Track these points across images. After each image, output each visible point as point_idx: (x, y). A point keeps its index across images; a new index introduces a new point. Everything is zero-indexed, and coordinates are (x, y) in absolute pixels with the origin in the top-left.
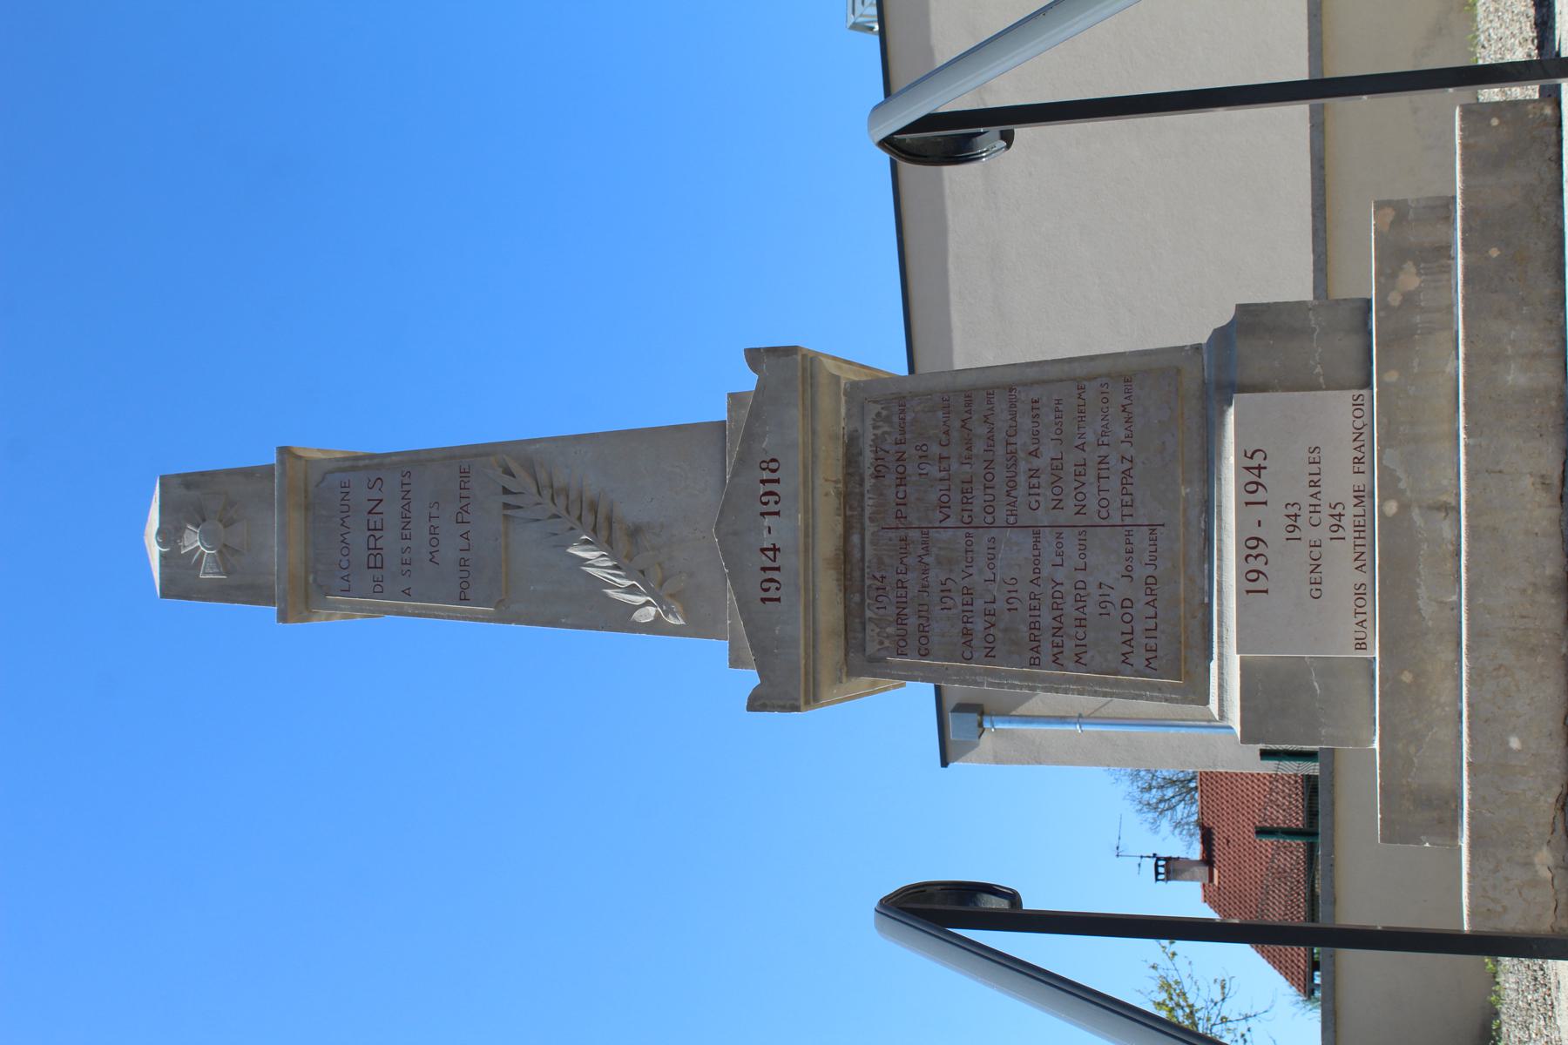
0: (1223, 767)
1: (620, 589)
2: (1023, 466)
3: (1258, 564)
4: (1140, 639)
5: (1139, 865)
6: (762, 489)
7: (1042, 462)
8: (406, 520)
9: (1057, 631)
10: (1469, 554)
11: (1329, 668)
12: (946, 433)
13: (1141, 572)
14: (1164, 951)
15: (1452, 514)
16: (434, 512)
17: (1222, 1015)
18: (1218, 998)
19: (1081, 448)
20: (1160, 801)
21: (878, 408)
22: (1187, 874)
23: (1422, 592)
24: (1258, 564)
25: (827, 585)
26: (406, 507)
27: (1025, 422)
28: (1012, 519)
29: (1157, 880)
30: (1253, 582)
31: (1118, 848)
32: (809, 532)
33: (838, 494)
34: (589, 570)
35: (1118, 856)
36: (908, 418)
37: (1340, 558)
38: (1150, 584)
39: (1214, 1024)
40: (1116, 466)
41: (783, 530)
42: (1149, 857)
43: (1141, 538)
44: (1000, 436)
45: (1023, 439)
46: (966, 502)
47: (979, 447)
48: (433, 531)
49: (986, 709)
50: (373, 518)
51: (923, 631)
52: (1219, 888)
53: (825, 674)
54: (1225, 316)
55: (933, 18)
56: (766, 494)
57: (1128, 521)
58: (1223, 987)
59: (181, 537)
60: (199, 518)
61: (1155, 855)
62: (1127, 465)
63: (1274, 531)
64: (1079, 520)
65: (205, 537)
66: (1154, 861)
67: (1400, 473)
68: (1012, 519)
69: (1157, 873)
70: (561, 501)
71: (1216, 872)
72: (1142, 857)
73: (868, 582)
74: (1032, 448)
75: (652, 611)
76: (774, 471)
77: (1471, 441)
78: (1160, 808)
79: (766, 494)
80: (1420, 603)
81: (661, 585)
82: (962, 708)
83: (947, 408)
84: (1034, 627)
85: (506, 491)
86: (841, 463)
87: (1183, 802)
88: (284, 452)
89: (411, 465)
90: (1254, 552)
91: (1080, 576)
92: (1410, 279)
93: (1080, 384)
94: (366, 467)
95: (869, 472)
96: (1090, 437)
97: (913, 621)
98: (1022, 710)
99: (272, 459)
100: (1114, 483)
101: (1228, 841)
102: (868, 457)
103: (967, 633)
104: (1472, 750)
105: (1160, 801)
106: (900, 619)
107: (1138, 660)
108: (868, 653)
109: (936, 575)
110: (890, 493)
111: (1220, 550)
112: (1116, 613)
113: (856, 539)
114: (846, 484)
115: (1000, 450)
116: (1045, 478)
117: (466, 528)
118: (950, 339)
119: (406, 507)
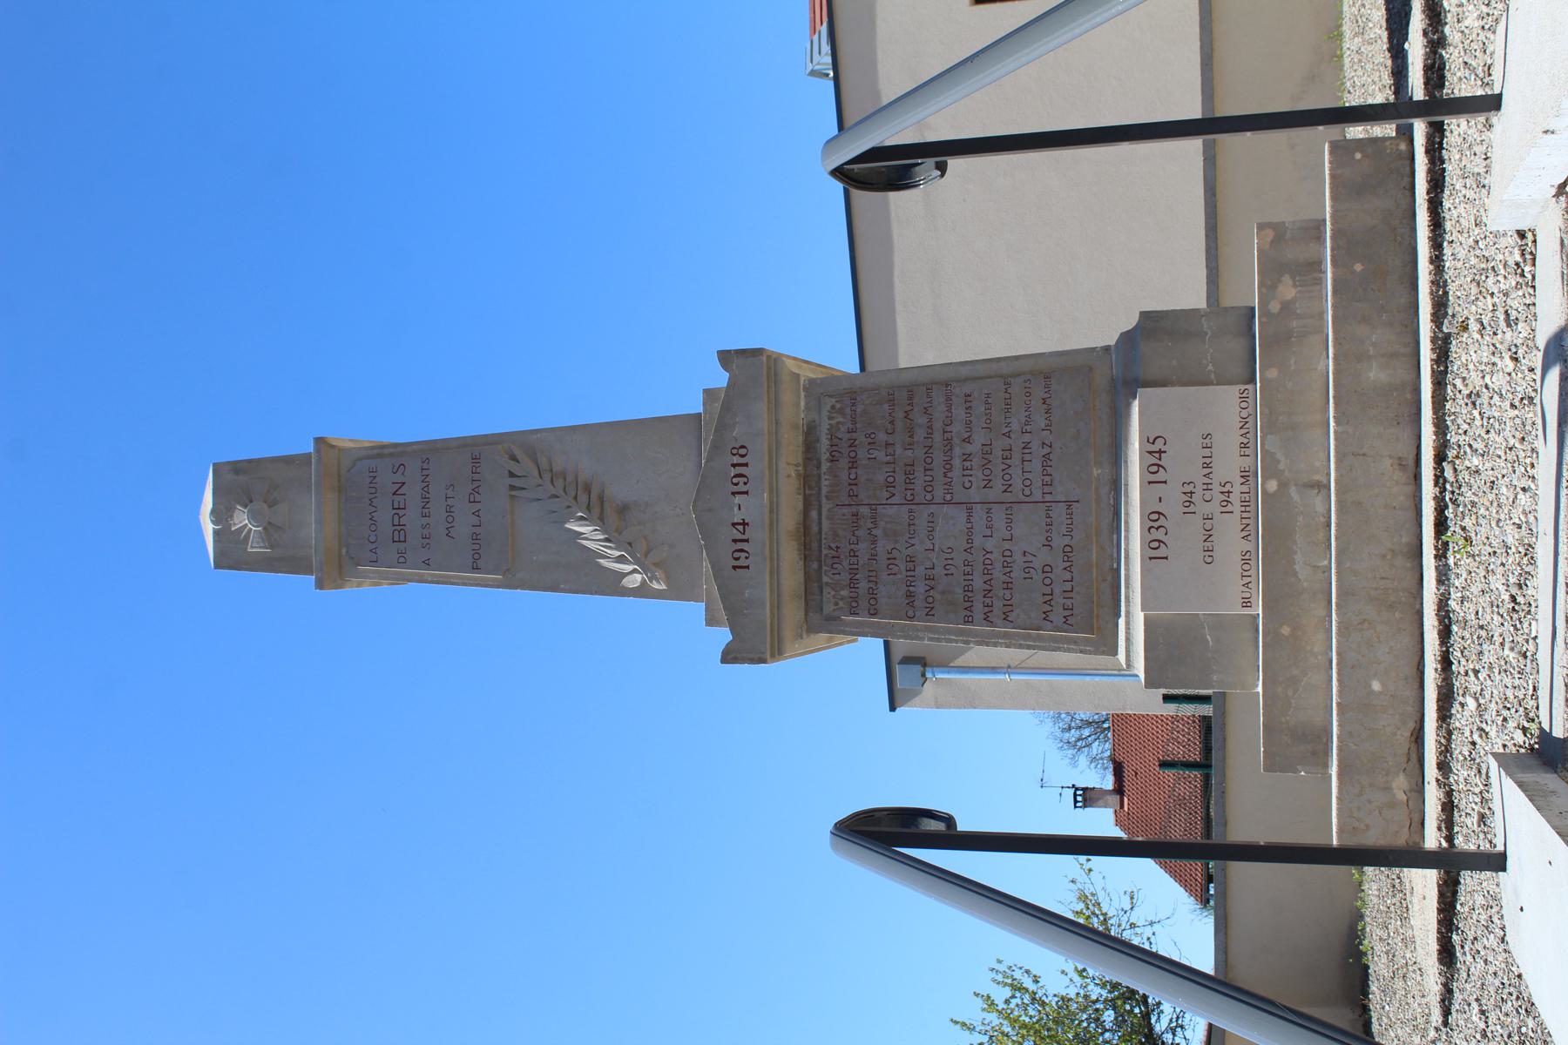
0: (1131, 710)
2: (957, 451)
3: (1159, 535)
4: (1059, 600)
6: (733, 472)
7: (974, 448)
8: (426, 500)
9: (987, 593)
10: (1338, 525)
11: (1220, 623)
12: (892, 422)
13: (1059, 542)
15: (1324, 491)
16: (450, 493)
18: (1127, 907)
19: (1008, 435)
20: (1079, 740)
22: (1101, 802)
23: (1298, 558)
24: (1159, 535)
25: (790, 554)
26: (426, 488)
27: (959, 412)
28: (948, 497)
29: (1075, 807)
30: (1155, 549)
31: (1042, 780)
32: (774, 509)
33: (799, 475)
34: (584, 542)
35: (1042, 787)
38: (1068, 552)
41: (751, 508)
42: (1069, 787)
43: (1059, 512)
44: (938, 425)
45: (957, 428)
47: (920, 435)
48: (449, 510)
49: (929, 660)
51: (872, 594)
52: (1129, 814)
53: (788, 633)
54: (1130, 322)
55: (880, 67)
56: (736, 476)
57: (1048, 498)
58: (1132, 898)
59: (232, 516)
61: (1073, 786)
62: (1047, 450)
63: (1173, 507)
64: (1007, 497)
65: (253, 516)
66: (1073, 791)
67: (1279, 456)
69: (1076, 801)
71: (1126, 800)
72: (1062, 787)
73: (824, 552)
74: (966, 435)
75: (638, 577)
78: (1078, 745)
79: (736, 476)
80: (1297, 567)
83: (892, 401)
84: (968, 589)
85: (512, 475)
86: (801, 449)
88: (320, 441)
89: (429, 453)
90: (1156, 524)
91: (1007, 545)
92: (1287, 290)
93: (1006, 380)
94: (391, 455)
95: (825, 456)
96: (1015, 426)
97: (863, 586)
98: (959, 662)
99: (310, 448)
100: (1036, 465)
102: (824, 443)
103: (910, 595)
104: (1340, 692)
105: (1079, 740)
109: (883, 546)
110: (844, 475)
111: (1127, 523)
112: (1038, 577)
113: (814, 514)
114: (805, 467)
116: (976, 462)
118: (895, 343)
119: (426, 488)
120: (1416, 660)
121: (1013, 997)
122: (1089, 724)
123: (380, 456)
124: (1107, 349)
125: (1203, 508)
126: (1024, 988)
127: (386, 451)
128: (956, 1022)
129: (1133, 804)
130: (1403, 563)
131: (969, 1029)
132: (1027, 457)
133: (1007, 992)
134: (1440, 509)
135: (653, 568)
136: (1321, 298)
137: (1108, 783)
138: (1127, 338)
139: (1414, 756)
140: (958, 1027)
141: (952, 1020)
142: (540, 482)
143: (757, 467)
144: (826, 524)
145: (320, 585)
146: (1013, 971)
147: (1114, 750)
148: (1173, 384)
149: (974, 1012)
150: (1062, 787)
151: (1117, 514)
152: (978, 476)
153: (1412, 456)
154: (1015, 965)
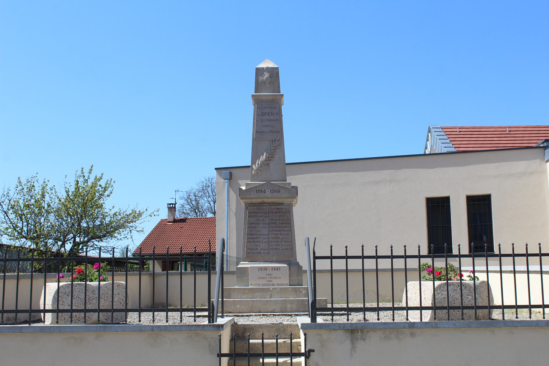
0: (217, 242)
1: (259, 162)
2: (278, 232)
3: (263, 270)
4: (252, 251)
5: (173, 198)
6: (275, 190)
7: (279, 236)
8: (270, 120)
9: (253, 238)
10: (264, 300)
11: (248, 280)
12: (284, 220)
13: (262, 251)
14: (152, 213)
15: (270, 298)
16: (272, 126)
17: (132, 231)
18: (138, 229)
19: (281, 242)
20: (191, 200)
21: (288, 208)
22: (170, 214)
23: (259, 293)
24: (263, 270)
25: (259, 201)
26: (273, 120)
27: (285, 233)
28: (270, 231)
29: (168, 204)
30: (261, 269)
31: (178, 191)
32: (268, 198)
33: (274, 202)
34: (262, 156)
35: (175, 191)
36: (286, 214)
37: (264, 282)
38: (260, 253)
39: (130, 229)
40: (278, 247)
41: (268, 193)
42: (175, 201)
43: (267, 251)
44: (283, 229)
45: (283, 232)
46: (273, 223)
47: (281, 225)
48: (268, 126)
49: (230, 180)
50: (271, 113)
51: (252, 216)
52: (166, 225)
53: (245, 200)
54: (301, 264)
55: (409, 170)
56: (274, 191)
57: (270, 249)
58: (141, 231)
59: (267, 72)
60: (271, 77)
61: (176, 203)
62: (278, 249)
63: (268, 272)
64: (270, 242)
65: (267, 78)
66: (174, 203)
67: (276, 290)
68: (270, 231)
69: (170, 204)
70: (273, 151)
71: (171, 224)
72: (175, 199)
73: (260, 207)
74: (281, 234)
75: (255, 168)
76: (278, 192)
77: (280, 300)
78: (188, 199)
79: (274, 191)
80: (257, 293)
81: (259, 170)
82: (231, 174)
83: (288, 220)
84: (253, 234)
85: (275, 140)
86: (279, 202)
87: (190, 208)
88: (283, 95)
89: (279, 121)
90: (265, 269)
91: (261, 242)
92: (304, 292)
93: (291, 242)
94: (280, 112)
95: (278, 207)
96: (283, 243)
97: (254, 215)
98: (231, 189)
99: (282, 93)
100: (276, 247)
101: (182, 228)
102: (280, 207)
103: (252, 224)
104: (237, 300)
105: (191, 200)
106: (254, 212)
107: (248, 251)
108: (249, 207)
109: (261, 218)
110: (274, 211)
111: (265, 263)
112: (256, 247)
113: (267, 205)
114: (276, 203)
115: (281, 229)
116: (276, 236)
117: (269, 132)
118: (327, 172)
119: (273, 120)
120: (242, 312)
121: (102, 188)
122: (198, 203)
123: (279, 110)
124: (296, 260)
125: (268, 277)
126: (105, 191)
127: (280, 111)
128: (92, 167)
129: (170, 227)
130: (258, 310)
131: (90, 172)
132: (277, 245)
133: (103, 186)
134: (266, 315)
135: (257, 171)
136: (302, 297)
137: (178, 216)
138: (298, 264)
139: (227, 312)
140: (90, 168)
141: (93, 165)
142: (274, 146)
143: (276, 194)
144: (265, 207)
145: (253, 96)
146: (111, 187)
147: (191, 219)
148: (289, 272)
149: (96, 173)
150: (175, 199)
151: (267, 262)
152: (274, 236)
153: (275, 312)
154: (113, 188)
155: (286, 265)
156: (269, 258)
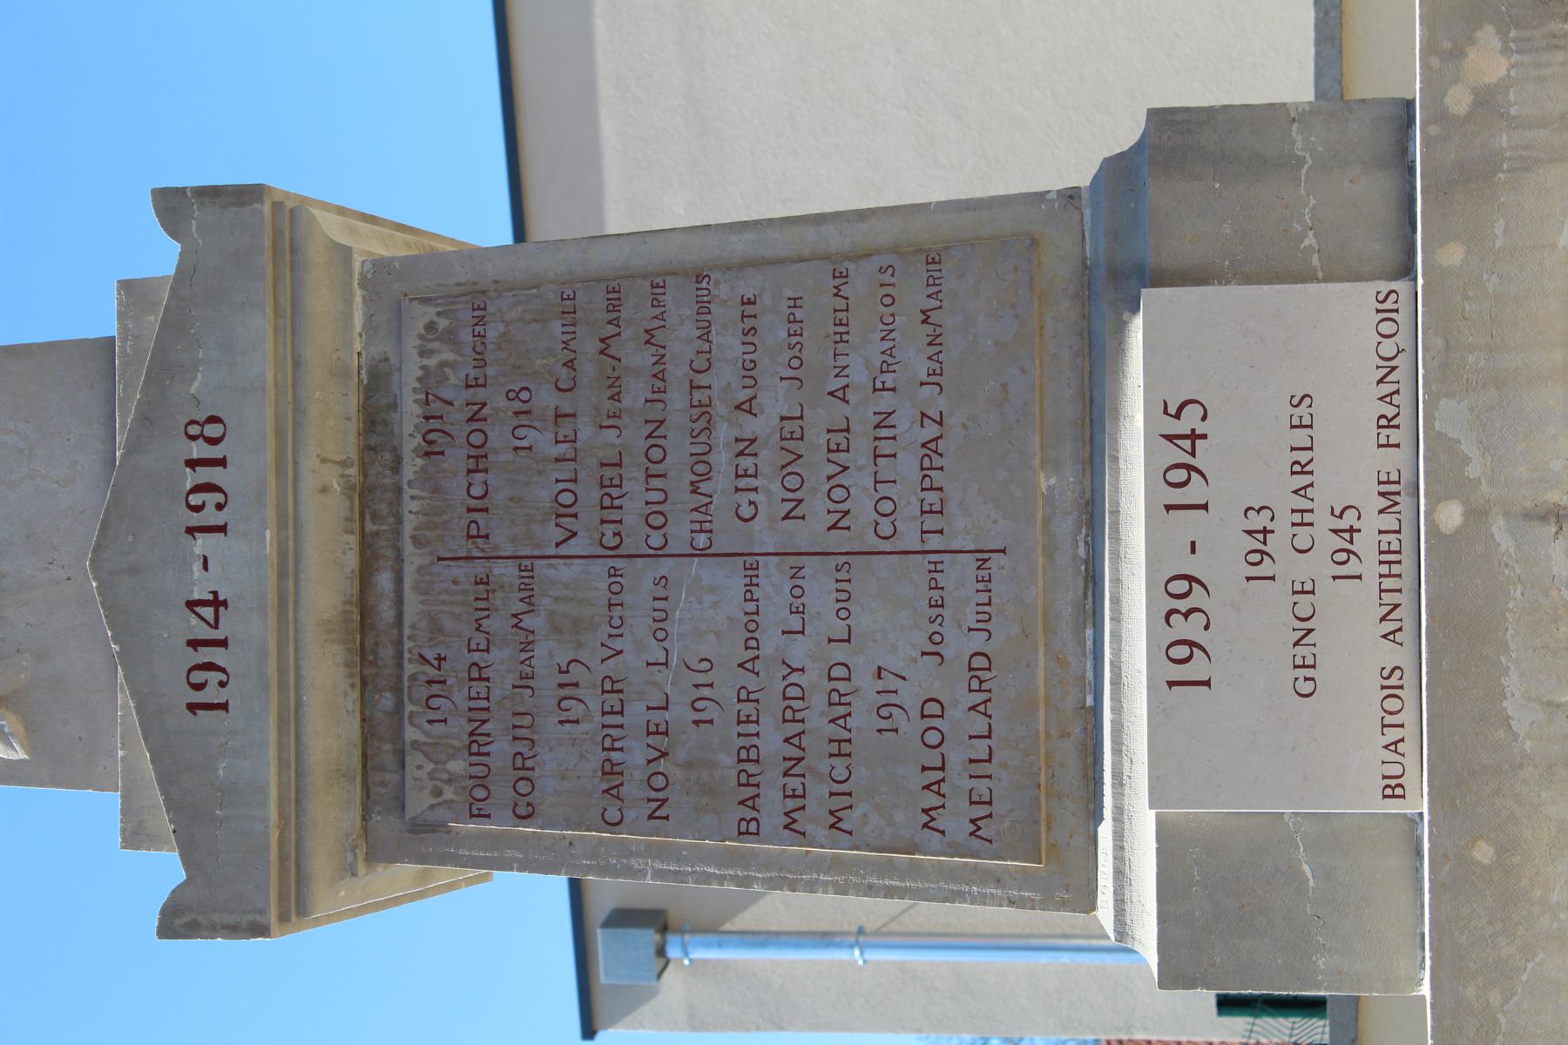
0: (1146, 1029)
2: (723, 433)
3: (1191, 629)
4: (958, 781)
6: (191, 478)
7: (763, 425)
12: (569, 364)
13: (959, 645)
19: (840, 395)
24: (1191, 629)
27: (728, 343)
28: (702, 540)
32: (288, 567)
33: (349, 488)
36: (492, 335)
38: (979, 669)
40: (910, 432)
43: (959, 575)
44: (678, 372)
45: (724, 377)
46: (610, 505)
47: (636, 392)
51: (523, 768)
53: (321, 862)
54: (1125, 133)
56: (198, 489)
57: (934, 542)
62: (931, 431)
64: (837, 540)
67: (1468, 447)
68: (702, 540)
73: (410, 668)
74: (743, 395)
79: (198, 489)
82: (623, 918)
83: (569, 315)
84: (747, 757)
86: (354, 426)
90: (1183, 605)
91: (839, 653)
95: (411, 443)
96: (859, 375)
97: (501, 749)
98: (743, 921)
100: (907, 467)
102: (410, 413)
103: (611, 770)
106: (476, 744)
107: (955, 822)
108: (410, 813)
109: (548, 654)
110: (456, 488)
111: (1116, 601)
112: (910, 726)
113: (384, 580)
114: (364, 472)
115: (677, 399)
116: (768, 457)
124: (1071, 196)
125: (1288, 567)
151: (1093, 580)
152: (771, 488)
155: (1137, 330)
156: (1050, 549)
